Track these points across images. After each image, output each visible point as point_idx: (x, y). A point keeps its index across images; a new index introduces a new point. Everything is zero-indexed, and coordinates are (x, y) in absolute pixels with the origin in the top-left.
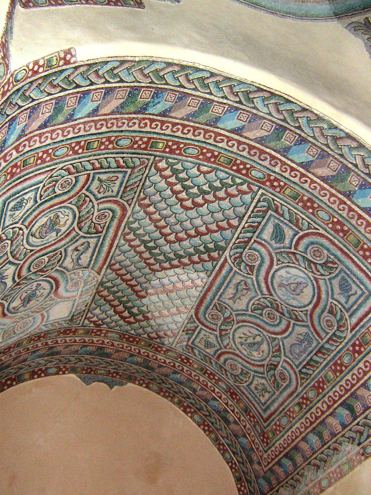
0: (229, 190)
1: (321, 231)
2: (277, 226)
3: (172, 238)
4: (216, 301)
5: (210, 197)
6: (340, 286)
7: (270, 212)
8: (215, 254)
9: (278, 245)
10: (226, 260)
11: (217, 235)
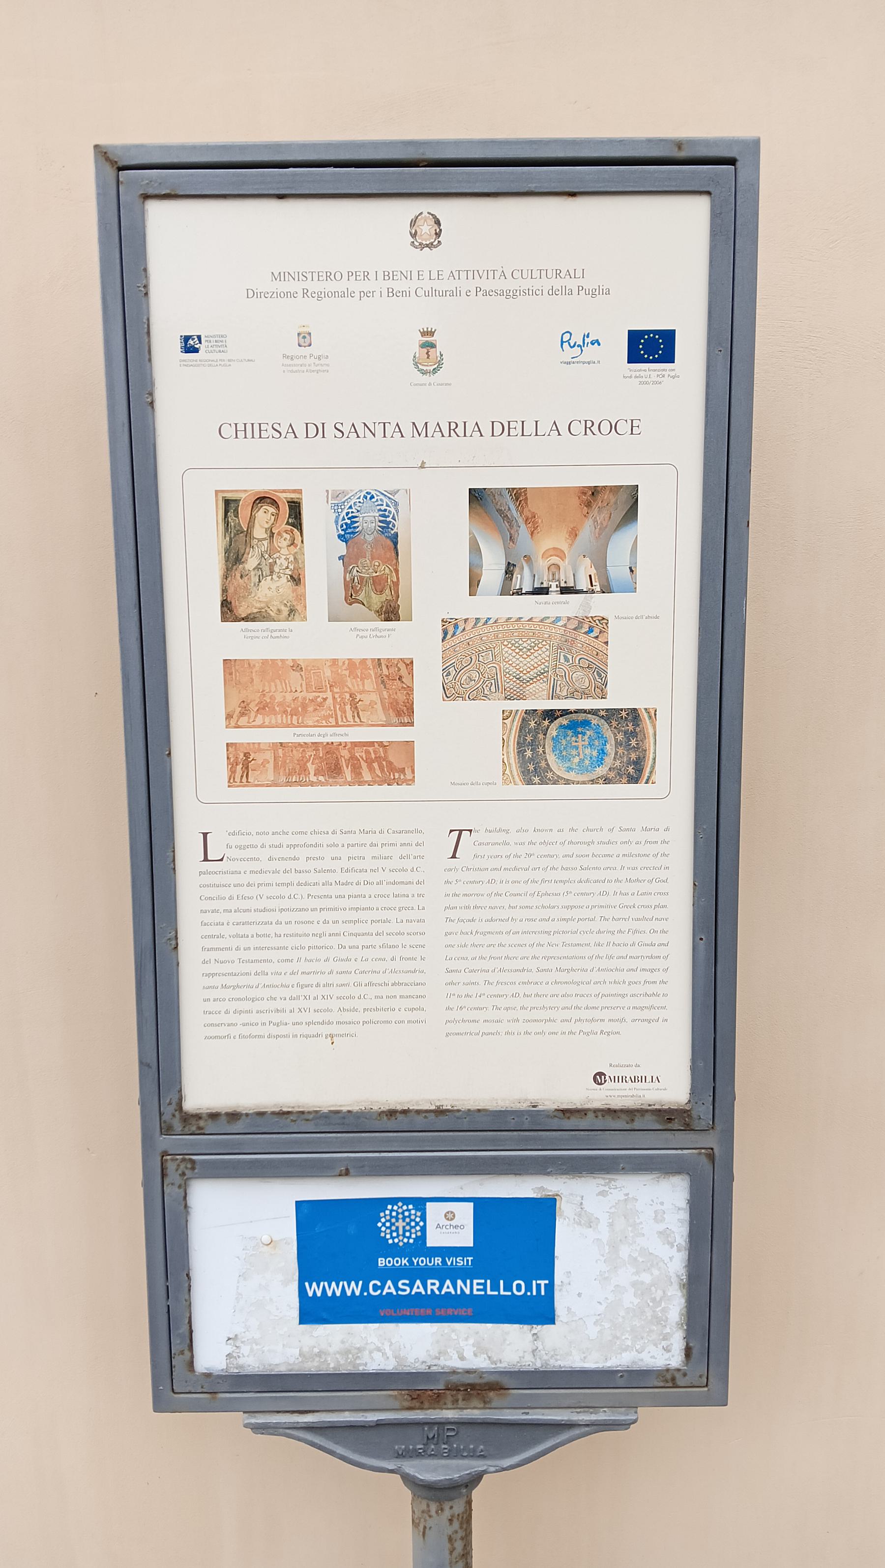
0: (539, 646)
1: (582, 653)
2: (564, 656)
3: (525, 672)
4: (554, 694)
5: (532, 651)
6: (597, 674)
7: (559, 650)
8: (545, 674)
9: (568, 664)
10: (551, 676)
11: (543, 666)
